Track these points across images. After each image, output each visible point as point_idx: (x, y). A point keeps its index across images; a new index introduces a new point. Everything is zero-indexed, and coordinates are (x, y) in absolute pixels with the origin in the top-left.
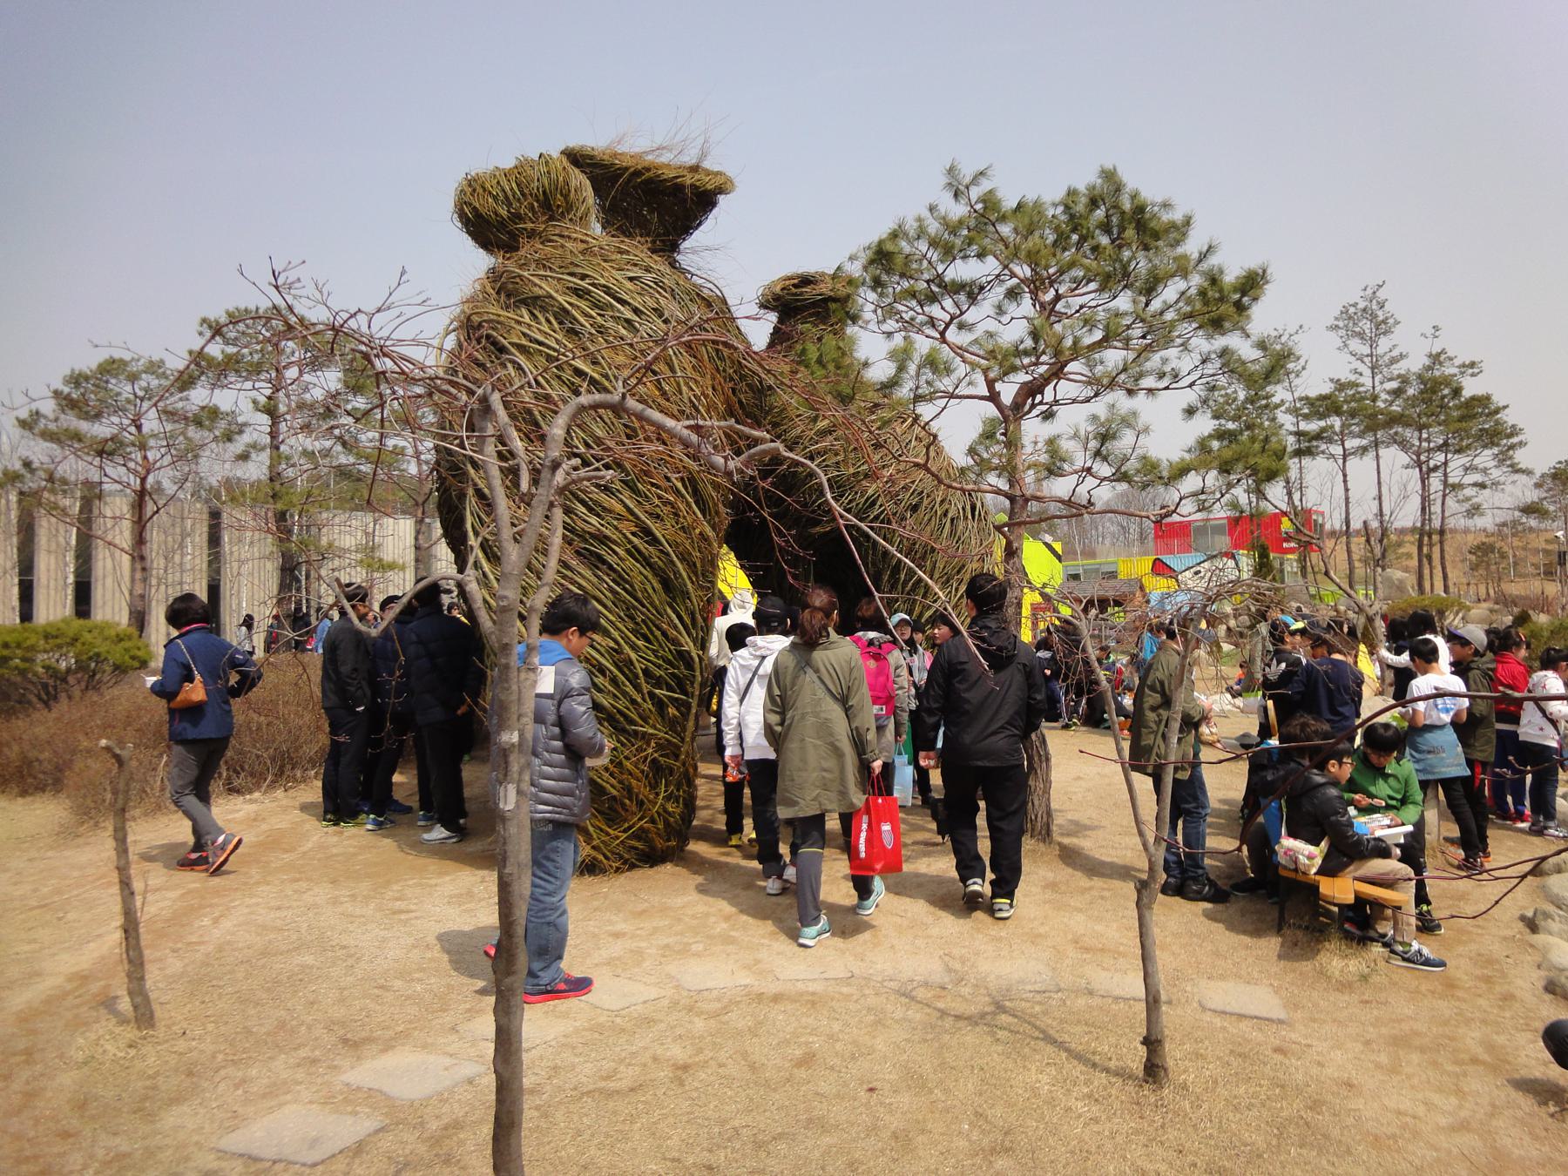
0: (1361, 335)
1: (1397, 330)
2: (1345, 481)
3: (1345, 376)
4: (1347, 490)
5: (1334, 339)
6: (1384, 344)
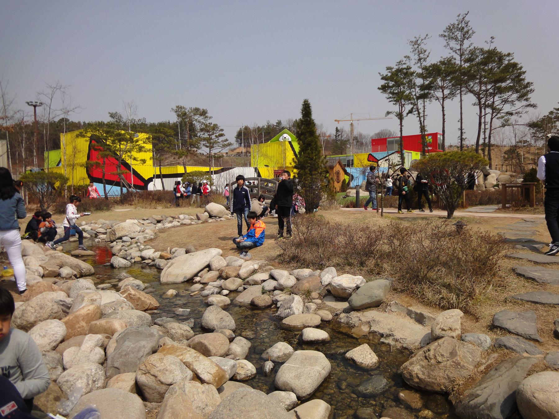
0: (456, 39)
2: (443, 111)
4: (444, 115)
5: (443, 41)
6: (466, 43)
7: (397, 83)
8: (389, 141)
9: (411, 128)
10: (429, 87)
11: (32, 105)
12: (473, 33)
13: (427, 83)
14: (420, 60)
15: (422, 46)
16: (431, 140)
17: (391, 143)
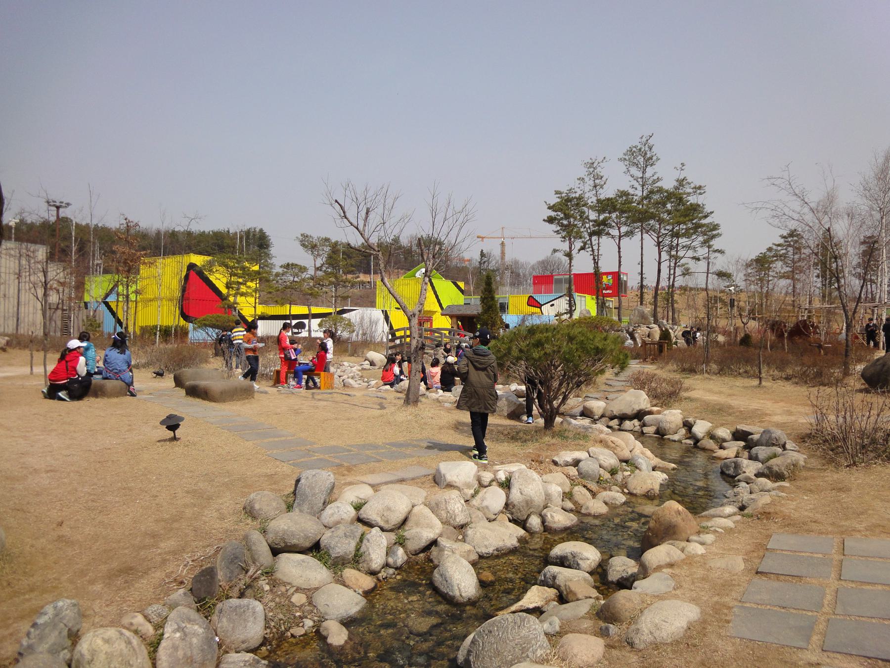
1: (658, 163)
2: (619, 252)
3: (625, 187)
4: (620, 257)
5: (622, 167)
6: (650, 171)
7: (566, 213)
8: (556, 280)
9: (583, 264)
10: (604, 223)
11: (54, 205)
12: (658, 159)
13: (602, 217)
14: (595, 186)
15: (599, 169)
16: (611, 282)
17: (559, 281)
